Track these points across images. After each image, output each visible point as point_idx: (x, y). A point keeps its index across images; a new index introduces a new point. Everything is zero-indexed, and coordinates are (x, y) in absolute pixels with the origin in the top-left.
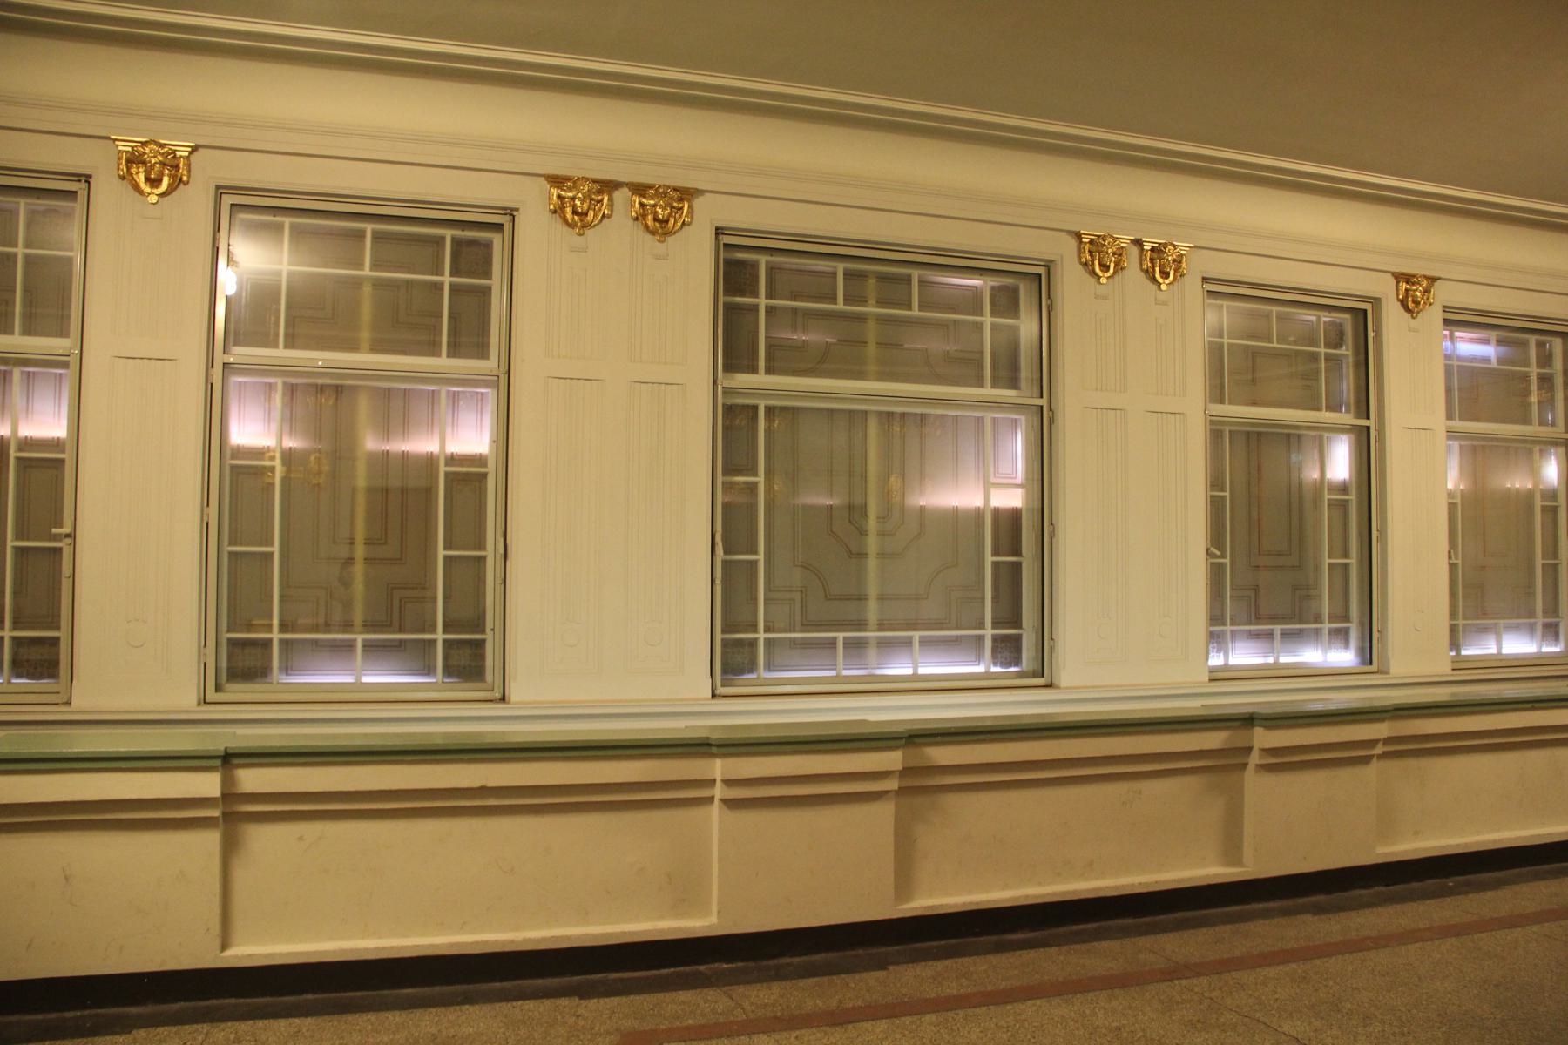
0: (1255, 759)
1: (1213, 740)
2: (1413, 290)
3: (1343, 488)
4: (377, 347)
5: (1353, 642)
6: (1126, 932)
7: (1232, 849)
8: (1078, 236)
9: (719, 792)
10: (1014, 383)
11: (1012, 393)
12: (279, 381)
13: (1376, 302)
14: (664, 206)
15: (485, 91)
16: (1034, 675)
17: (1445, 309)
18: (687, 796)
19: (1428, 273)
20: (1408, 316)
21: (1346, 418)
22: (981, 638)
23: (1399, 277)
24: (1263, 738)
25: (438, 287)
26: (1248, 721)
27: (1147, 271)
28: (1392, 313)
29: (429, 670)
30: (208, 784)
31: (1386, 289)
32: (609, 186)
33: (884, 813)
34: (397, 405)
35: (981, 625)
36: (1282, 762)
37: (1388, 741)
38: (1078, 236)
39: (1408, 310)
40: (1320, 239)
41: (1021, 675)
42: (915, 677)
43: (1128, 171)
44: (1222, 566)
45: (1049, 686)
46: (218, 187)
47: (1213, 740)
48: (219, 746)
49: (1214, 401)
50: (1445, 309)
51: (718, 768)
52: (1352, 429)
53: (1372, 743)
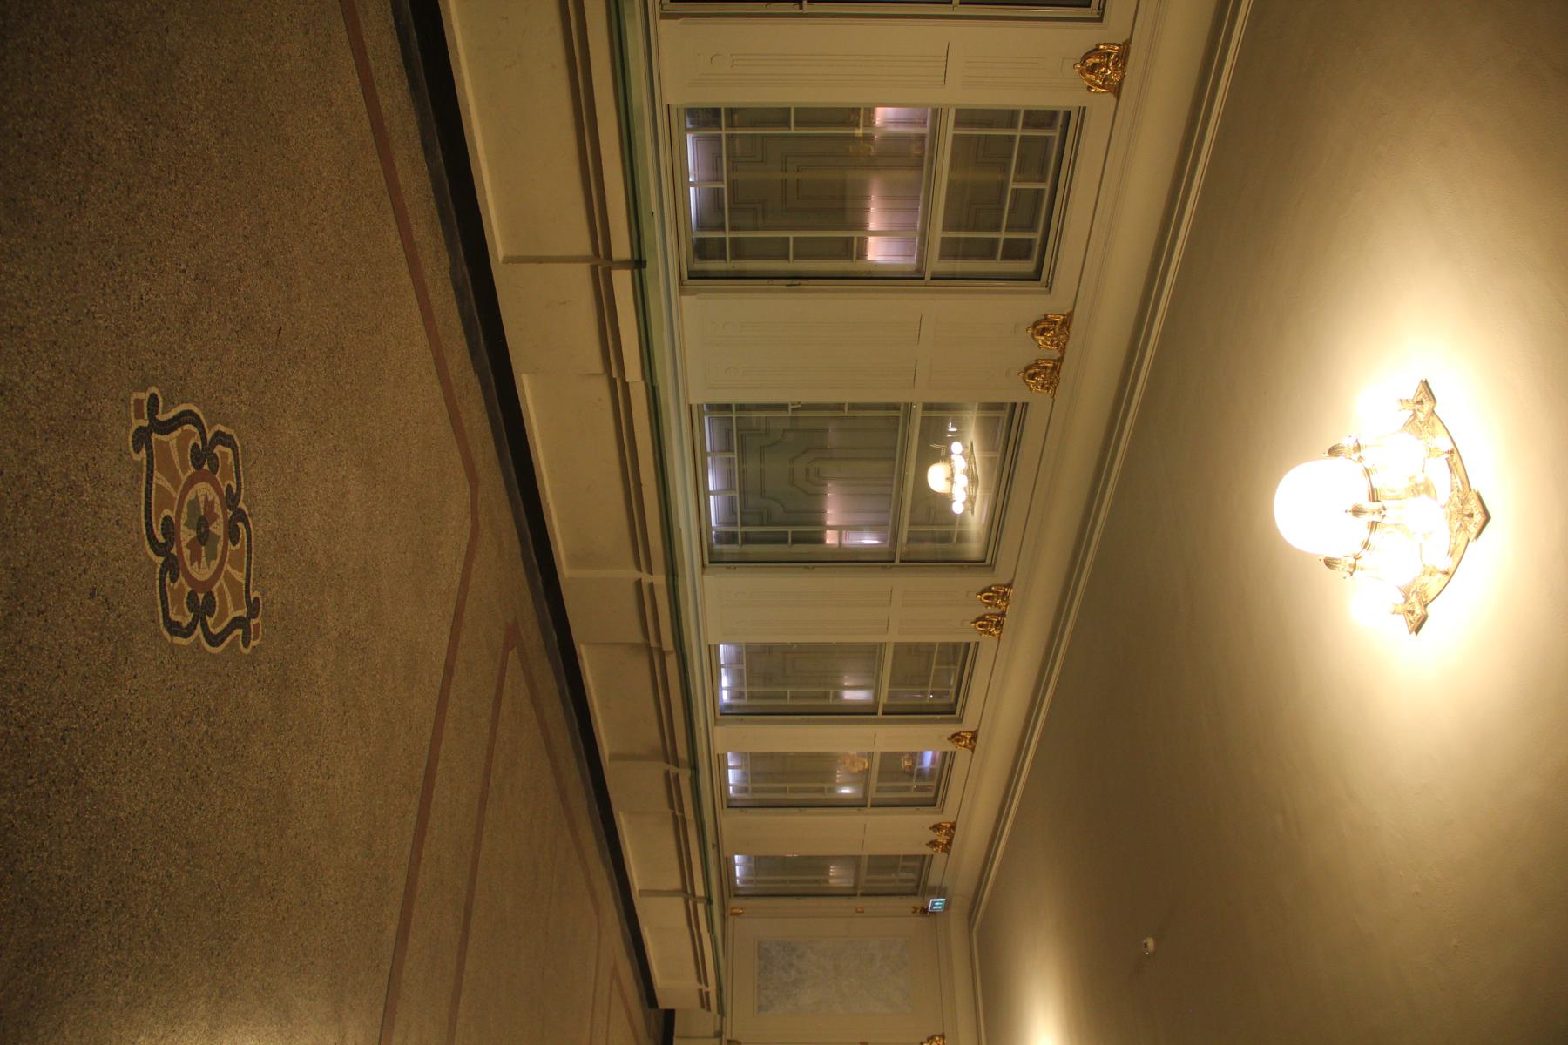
0: (673, 770)
1: (683, 753)
2: (1107, 66)
3: (837, 696)
4: (950, 184)
5: (735, 702)
6: (525, 558)
7: (615, 757)
8: (1010, 586)
9: (646, 579)
10: (909, 540)
11: (905, 540)
12: (926, 131)
13: (960, 720)
14: (1047, 374)
15: (1019, 727)
16: (711, 553)
17: (1025, 405)
18: (641, 555)
19: (1069, 345)
20: (1022, 368)
21: (883, 699)
22: (735, 524)
23: (1126, 47)
24: (685, 776)
25: (997, 228)
26: (694, 767)
27: (1097, 49)
28: (953, 729)
29: (701, 226)
30: (621, 248)
31: (969, 724)
32: (1063, 350)
33: (638, 638)
34: (903, 199)
35: (743, 524)
36: (671, 783)
37: (683, 818)
38: (1010, 586)
39: (1087, 56)
40: (1003, 694)
41: (710, 546)
42: (707, 493)
43: (1003, 789)
44: (787, 124)
45: (703, 566)
46: (1100, 20)
47: (683, 753)
48: (648, 256)
49: (959, 112)
50: (953, 754)
51: (659, 579)
52: (865, 798)
53: (682, 810)
